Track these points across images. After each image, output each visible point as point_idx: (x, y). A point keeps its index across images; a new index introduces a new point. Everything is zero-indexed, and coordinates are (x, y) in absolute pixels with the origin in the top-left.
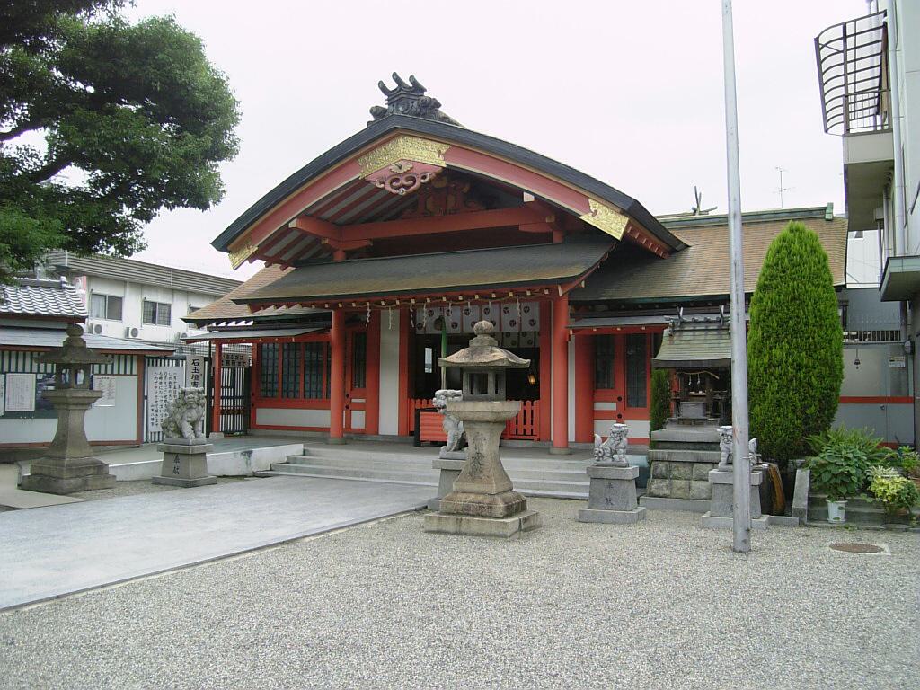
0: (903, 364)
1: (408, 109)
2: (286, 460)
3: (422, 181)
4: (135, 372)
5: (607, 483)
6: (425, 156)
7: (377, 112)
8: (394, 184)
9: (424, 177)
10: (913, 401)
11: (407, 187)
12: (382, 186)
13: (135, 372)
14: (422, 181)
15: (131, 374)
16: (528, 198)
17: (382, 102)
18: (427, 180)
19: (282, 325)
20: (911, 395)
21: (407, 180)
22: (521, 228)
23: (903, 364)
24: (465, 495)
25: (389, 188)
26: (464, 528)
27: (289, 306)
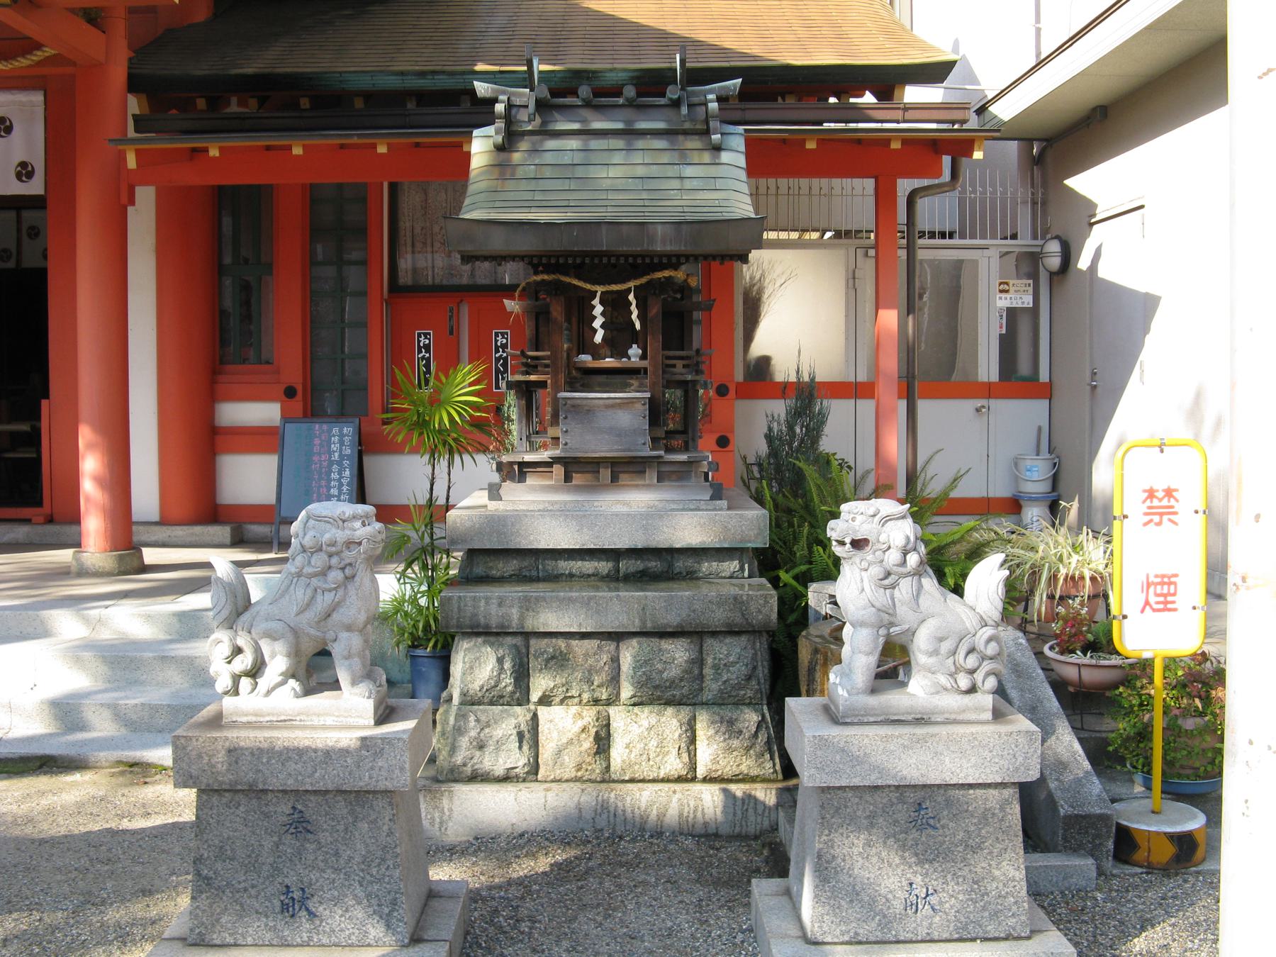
0: (1028, 301)
10: (1046, 392)
20: (1044, 376)
23: (1028, 301)
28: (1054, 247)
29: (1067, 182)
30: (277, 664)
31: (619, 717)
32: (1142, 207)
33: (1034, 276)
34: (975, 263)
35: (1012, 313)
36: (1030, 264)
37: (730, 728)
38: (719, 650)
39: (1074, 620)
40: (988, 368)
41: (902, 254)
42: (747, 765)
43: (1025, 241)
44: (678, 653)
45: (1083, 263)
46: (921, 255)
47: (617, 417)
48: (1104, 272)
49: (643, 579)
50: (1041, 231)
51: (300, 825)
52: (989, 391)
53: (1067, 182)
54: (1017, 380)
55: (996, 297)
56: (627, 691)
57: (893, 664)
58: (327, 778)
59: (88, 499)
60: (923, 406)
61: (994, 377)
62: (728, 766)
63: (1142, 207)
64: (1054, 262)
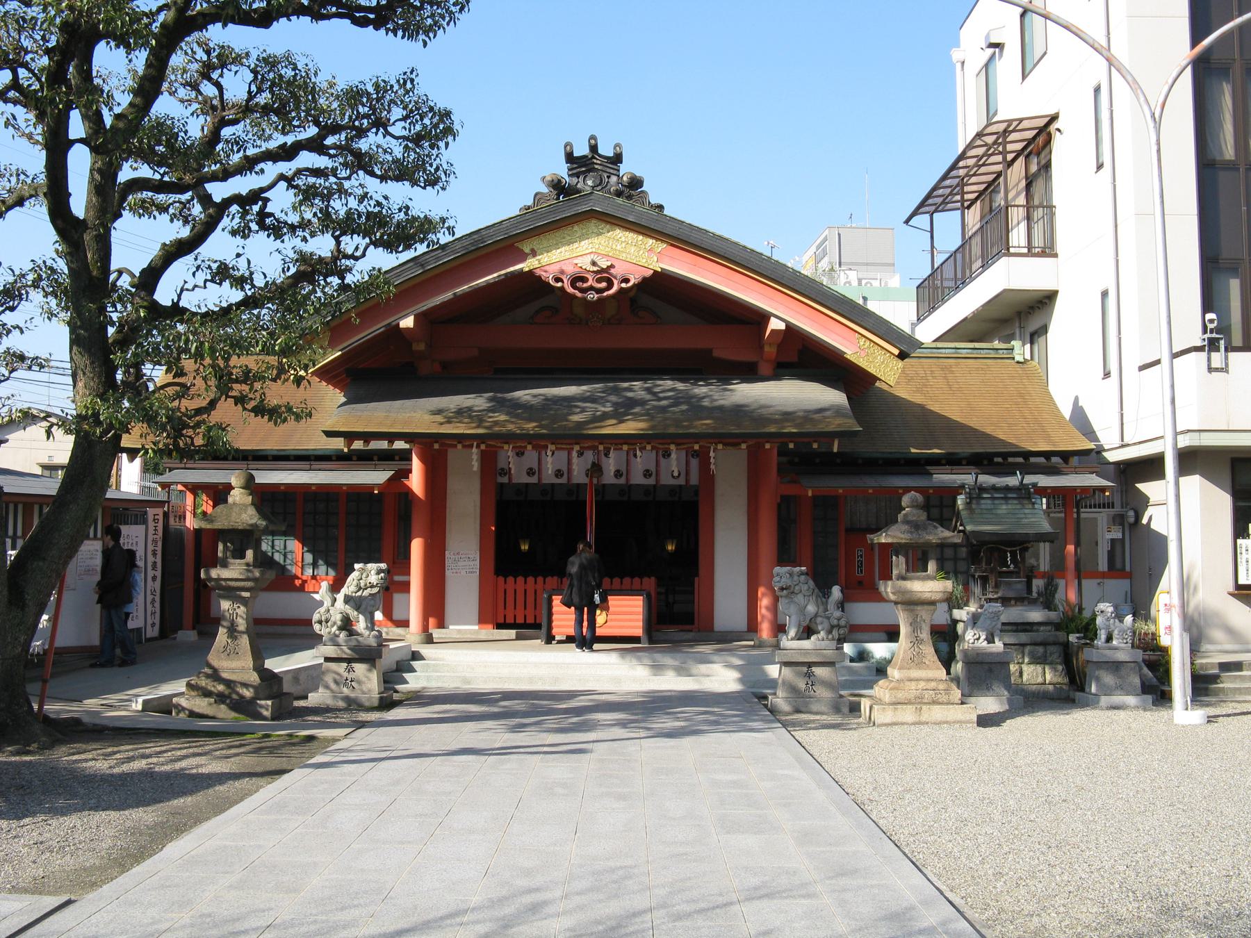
0: (1120, 536)
1: (593, 187)
2: (395, 667)
3: (624, 285)
4: (99, 535)
5: (986, 667)
6: (628, 255)
7: (558, 186)
8: (579, 284)
9: (627, 280)
10: (1129, 576)
11: (599, 291)
12: (559, 284)
13: (99, 535)
14: (624, 285)
15: (95, 537)
16: (775, 325)
17: (562, 170)
18: (630, 284)
19: (316, 465)
20: (1128, 569)
21: (599, 281)
22: (716, 354)
23: (1120, 536)
24: (913, 683)
25: (570, 290)
26: (923, 719)
27: (367, 442)
28: (1131, 513)
29: (1140, 486)
30: (983, 637)
31: (1025, 667)
32: (1142, 368)
33: (1122, 524)
34: (1096, 519)
35: (1113, 540)
36: (1119, 520)
37: (1055, 670)
38: (1051, 649)
39: (1147, 643)
40: (1103, 565)
41: (1075, 515)
42: (1060, 680)
43: (1117, 509)
44: (1041, 649)
45: (1144, 521)
46: (1083, 515)
47: (625, 612)
48: (1153, 526)
49: (1025, 631)
50: (1124, 504)
51: (990, 670)
52: (1103, 575)
53: (1140, 486)
54: (1115, 570)
55: (1107, 534)
56: (1026, 660)
57: (1109, 639)
58: (998, 660)
59: (763, 616)
60: (1084, 582)
61: (1106, 569)
62: (1055, 680)
63: (1142, 368)
64: (1132, 520)
